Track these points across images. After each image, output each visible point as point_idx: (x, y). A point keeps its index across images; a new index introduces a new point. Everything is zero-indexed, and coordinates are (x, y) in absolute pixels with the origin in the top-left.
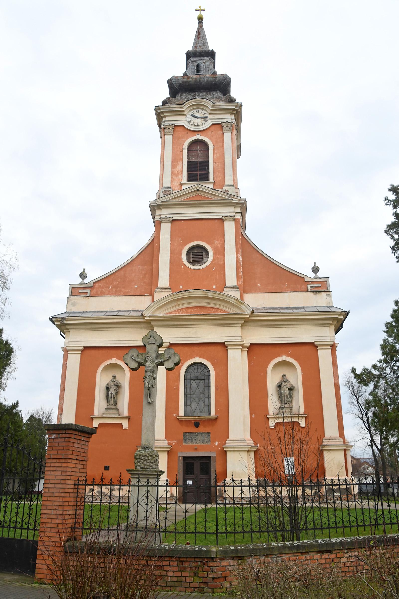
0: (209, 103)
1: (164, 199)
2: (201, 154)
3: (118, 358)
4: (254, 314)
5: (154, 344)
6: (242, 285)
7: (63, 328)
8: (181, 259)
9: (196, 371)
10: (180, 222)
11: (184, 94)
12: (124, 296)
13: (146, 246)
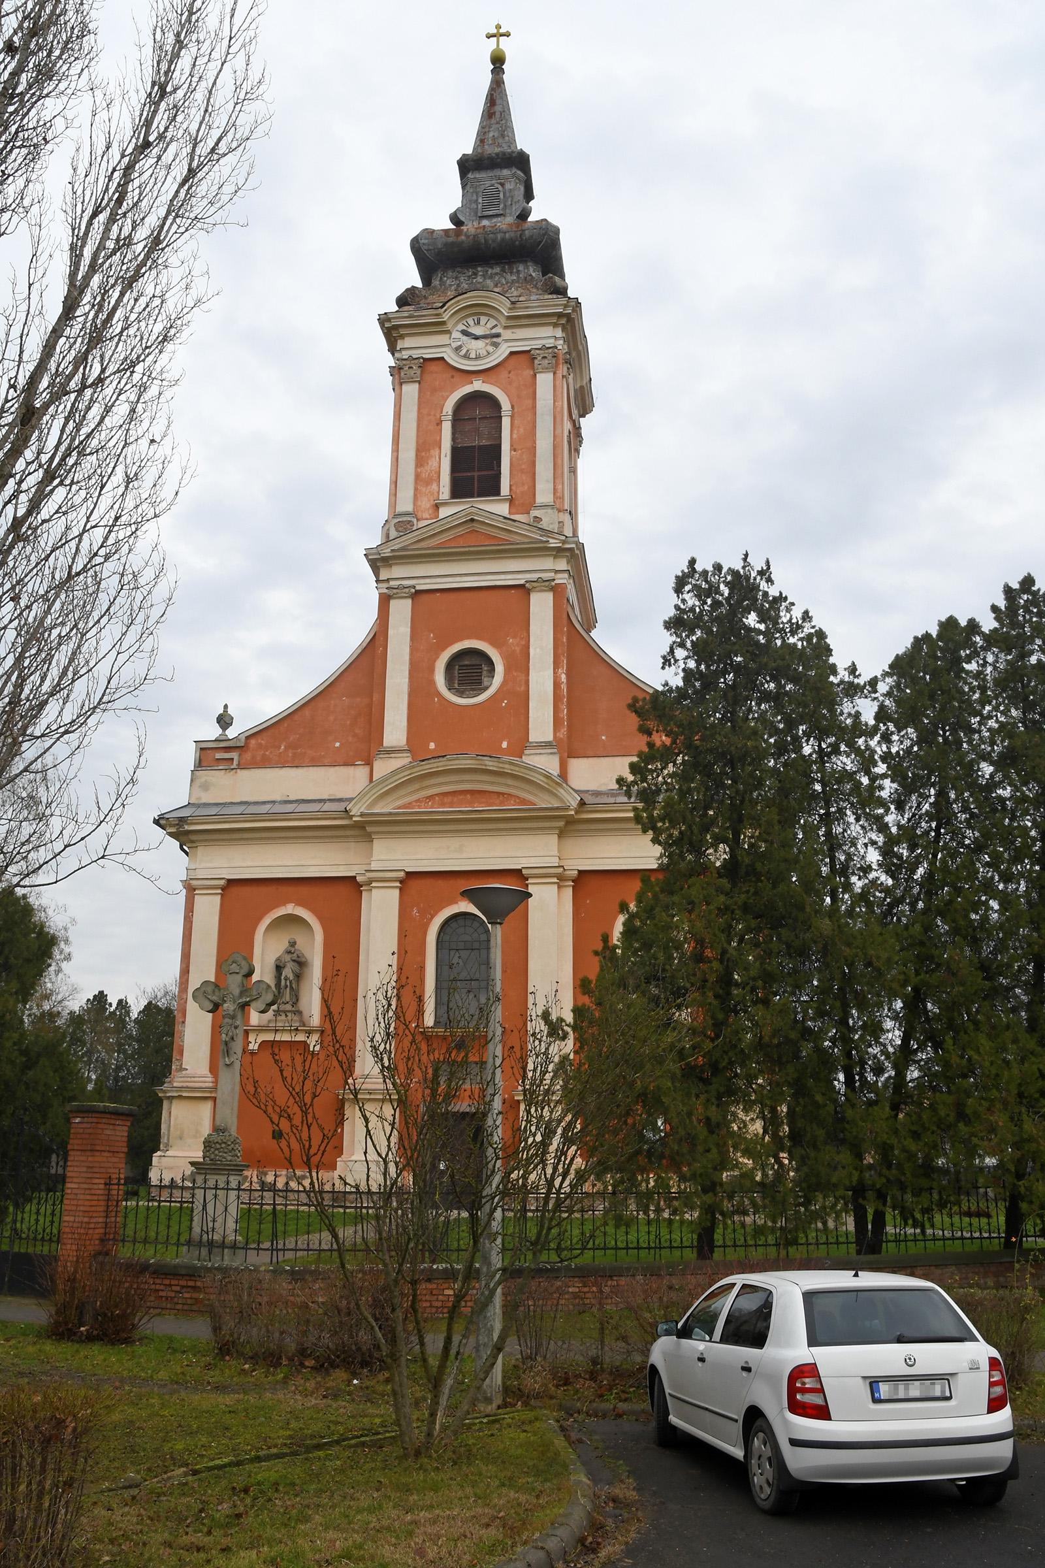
0: (501, 302)
3: (300, 903)
4: (588, 808)
6: (565, 739)
7: (184, 838)
8: (432, 683)
10: (432, 596)
13: (359, 651)
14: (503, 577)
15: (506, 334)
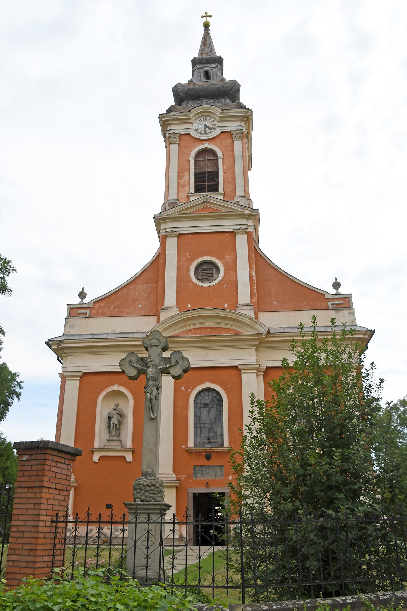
1: (171, 212)
2: (210, 164)
3: (120, 385)
4: (270, 335)
5: (157, 346)
6: (257, 303)
7: (60, 352)
8: (189, 276)
9: (206, 398)
11: (190, 102)
15: (220, 124)
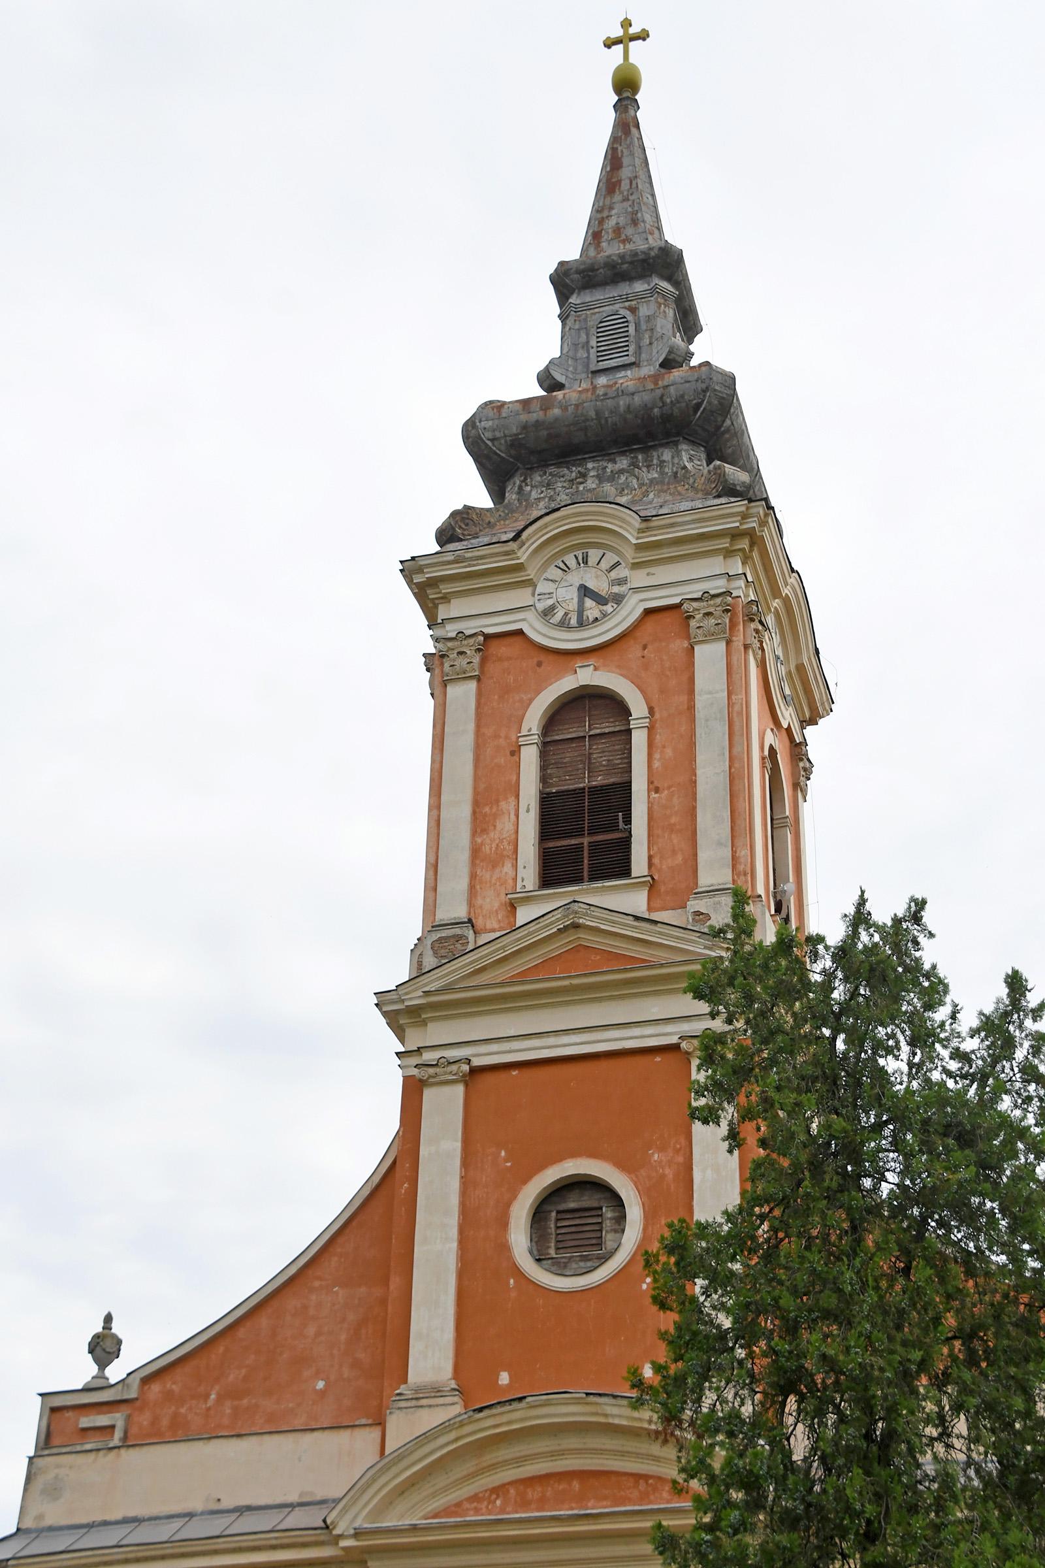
1: (433, 982)
2: (601, 754)
8: (504, 1248)
10: (502, 1076)
11: (537, 478)
12: (266, 1438)
14: (637, 1031)
15: (639, 578)
